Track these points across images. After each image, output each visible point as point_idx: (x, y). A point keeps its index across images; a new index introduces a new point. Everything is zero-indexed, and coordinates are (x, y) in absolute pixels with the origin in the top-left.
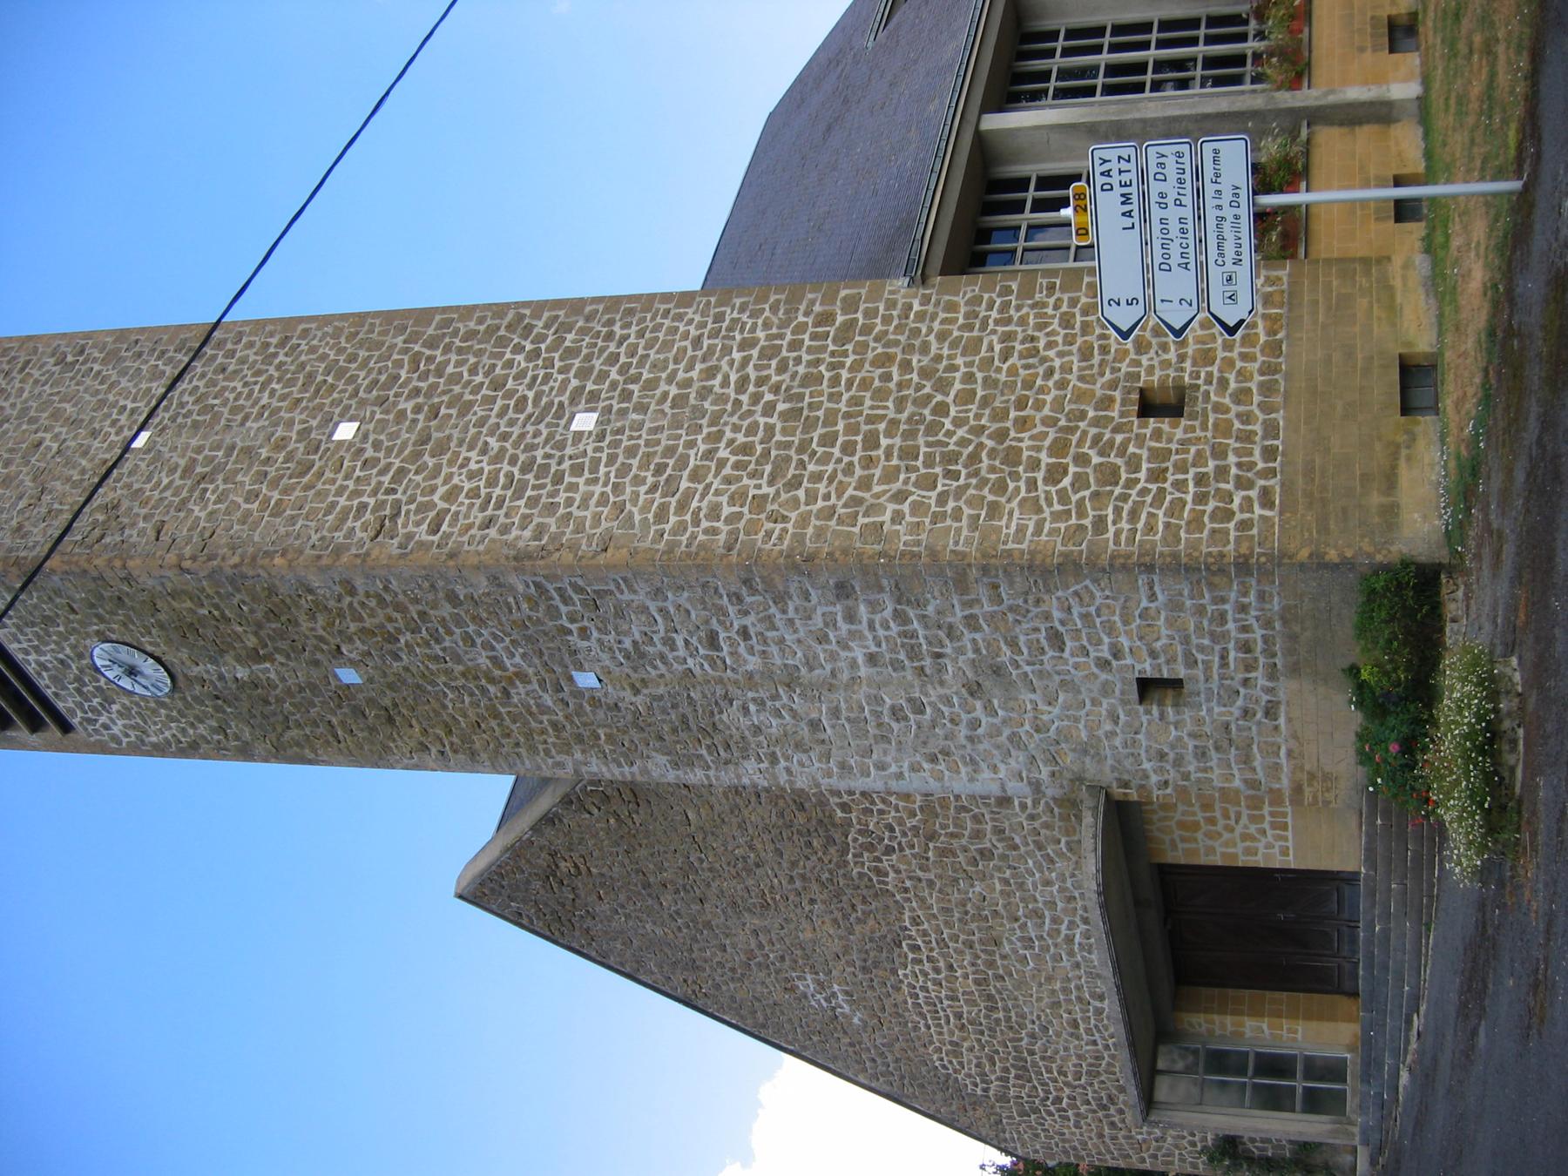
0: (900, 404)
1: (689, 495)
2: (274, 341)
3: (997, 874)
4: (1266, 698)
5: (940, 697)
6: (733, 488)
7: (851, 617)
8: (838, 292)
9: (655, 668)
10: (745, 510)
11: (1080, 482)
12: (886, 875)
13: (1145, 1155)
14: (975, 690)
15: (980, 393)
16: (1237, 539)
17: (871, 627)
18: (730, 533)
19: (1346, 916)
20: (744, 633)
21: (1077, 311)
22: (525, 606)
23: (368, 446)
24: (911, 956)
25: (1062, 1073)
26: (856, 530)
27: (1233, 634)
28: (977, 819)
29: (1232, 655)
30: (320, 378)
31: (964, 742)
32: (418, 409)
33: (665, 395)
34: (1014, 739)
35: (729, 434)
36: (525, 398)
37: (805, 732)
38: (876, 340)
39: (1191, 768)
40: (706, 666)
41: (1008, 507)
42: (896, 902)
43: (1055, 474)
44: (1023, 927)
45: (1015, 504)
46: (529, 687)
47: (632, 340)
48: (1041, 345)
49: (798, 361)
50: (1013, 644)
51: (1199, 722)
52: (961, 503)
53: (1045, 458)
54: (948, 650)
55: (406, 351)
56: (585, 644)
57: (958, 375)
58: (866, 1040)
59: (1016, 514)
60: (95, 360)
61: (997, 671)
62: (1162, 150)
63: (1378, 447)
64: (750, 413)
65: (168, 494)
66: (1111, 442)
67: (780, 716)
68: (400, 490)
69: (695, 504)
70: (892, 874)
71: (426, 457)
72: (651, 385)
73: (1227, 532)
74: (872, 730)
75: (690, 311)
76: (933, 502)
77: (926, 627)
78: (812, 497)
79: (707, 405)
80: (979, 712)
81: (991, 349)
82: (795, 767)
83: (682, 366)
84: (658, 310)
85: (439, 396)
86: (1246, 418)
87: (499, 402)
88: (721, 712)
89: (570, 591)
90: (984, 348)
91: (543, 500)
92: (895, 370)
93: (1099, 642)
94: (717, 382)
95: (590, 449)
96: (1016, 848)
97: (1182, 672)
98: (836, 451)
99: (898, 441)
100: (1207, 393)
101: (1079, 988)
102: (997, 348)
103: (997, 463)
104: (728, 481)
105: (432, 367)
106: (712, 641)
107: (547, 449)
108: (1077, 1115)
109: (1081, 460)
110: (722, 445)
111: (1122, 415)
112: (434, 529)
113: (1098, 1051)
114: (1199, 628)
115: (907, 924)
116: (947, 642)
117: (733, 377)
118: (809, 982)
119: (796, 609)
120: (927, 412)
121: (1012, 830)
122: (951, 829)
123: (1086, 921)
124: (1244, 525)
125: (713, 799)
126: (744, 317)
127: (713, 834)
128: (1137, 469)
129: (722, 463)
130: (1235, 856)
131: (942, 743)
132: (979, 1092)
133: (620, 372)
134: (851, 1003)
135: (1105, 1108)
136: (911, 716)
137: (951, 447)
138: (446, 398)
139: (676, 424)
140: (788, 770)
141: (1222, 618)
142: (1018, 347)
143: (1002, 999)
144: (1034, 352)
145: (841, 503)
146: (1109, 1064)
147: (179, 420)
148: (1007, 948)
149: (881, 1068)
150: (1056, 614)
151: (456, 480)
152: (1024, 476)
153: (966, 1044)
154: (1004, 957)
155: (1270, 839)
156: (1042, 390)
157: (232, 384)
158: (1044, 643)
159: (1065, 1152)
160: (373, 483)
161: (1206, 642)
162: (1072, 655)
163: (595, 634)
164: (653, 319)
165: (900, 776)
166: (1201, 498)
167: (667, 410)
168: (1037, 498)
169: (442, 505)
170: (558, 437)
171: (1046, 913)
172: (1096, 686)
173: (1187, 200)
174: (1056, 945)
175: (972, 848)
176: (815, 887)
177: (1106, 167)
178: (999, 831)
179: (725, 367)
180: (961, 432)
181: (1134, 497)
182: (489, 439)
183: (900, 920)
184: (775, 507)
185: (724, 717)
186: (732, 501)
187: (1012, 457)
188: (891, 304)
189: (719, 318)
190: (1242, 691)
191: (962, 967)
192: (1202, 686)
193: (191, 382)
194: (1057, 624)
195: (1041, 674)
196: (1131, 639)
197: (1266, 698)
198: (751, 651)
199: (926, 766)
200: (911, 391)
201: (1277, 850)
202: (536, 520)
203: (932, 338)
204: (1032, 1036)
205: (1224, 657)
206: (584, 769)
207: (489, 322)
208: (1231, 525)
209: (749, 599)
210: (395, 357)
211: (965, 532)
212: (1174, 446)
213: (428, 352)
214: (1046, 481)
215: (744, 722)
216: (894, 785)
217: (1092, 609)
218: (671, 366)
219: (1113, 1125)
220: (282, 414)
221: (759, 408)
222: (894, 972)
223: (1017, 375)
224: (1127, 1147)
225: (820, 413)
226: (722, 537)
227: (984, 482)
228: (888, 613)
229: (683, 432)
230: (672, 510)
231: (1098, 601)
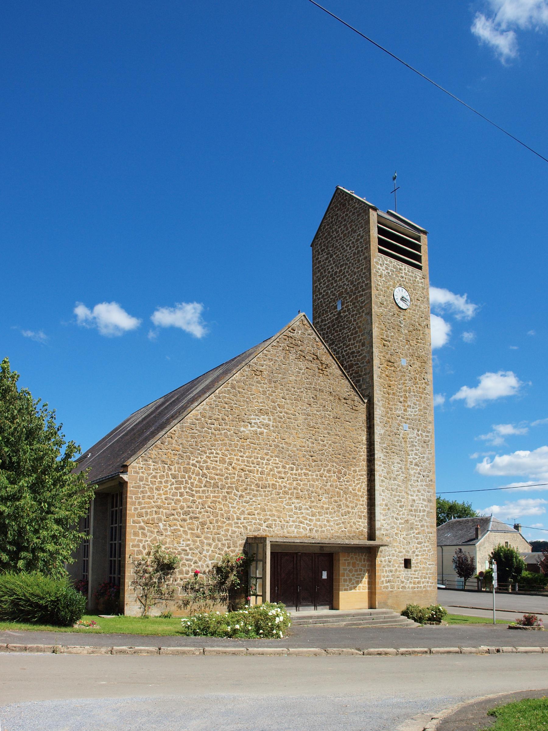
3: (331, 507)
5: (404, 513)
7: (423, 500)
9: (410, 447)
12: (327, 472)
14: (407, 521)
17: (422, 504)
24: (288, 466)
34: (393, 527)
46: (403, 410)
50: (419, 533)
54: (417, 519)
61: (412, 528)
80: (400, 521)
93: (419, 552)
106: (416, 465)
113: (233, 519)
114: (423, 573)
116: (419, 519)
122: (349, 499)
131: (391, 509)
136: (399, 504)
141: (425, 578)
150: (426, 544)
153: (230, 468)
154: (290, 498)
158: (419, 540)
162: (416, 546)
165: (381, 495)
171: (314, 518)
172: (408, 549)
176: (320, 447)
183: (307, 469)
185: (396, 457)
191: (282, 482)
192: (409, 573)
198: (415, 473)
201: (346, 588)
204: (241, 496)
209: (428, 479)
217: (427, 552)
222: (276, 456)
231: (429, 554)
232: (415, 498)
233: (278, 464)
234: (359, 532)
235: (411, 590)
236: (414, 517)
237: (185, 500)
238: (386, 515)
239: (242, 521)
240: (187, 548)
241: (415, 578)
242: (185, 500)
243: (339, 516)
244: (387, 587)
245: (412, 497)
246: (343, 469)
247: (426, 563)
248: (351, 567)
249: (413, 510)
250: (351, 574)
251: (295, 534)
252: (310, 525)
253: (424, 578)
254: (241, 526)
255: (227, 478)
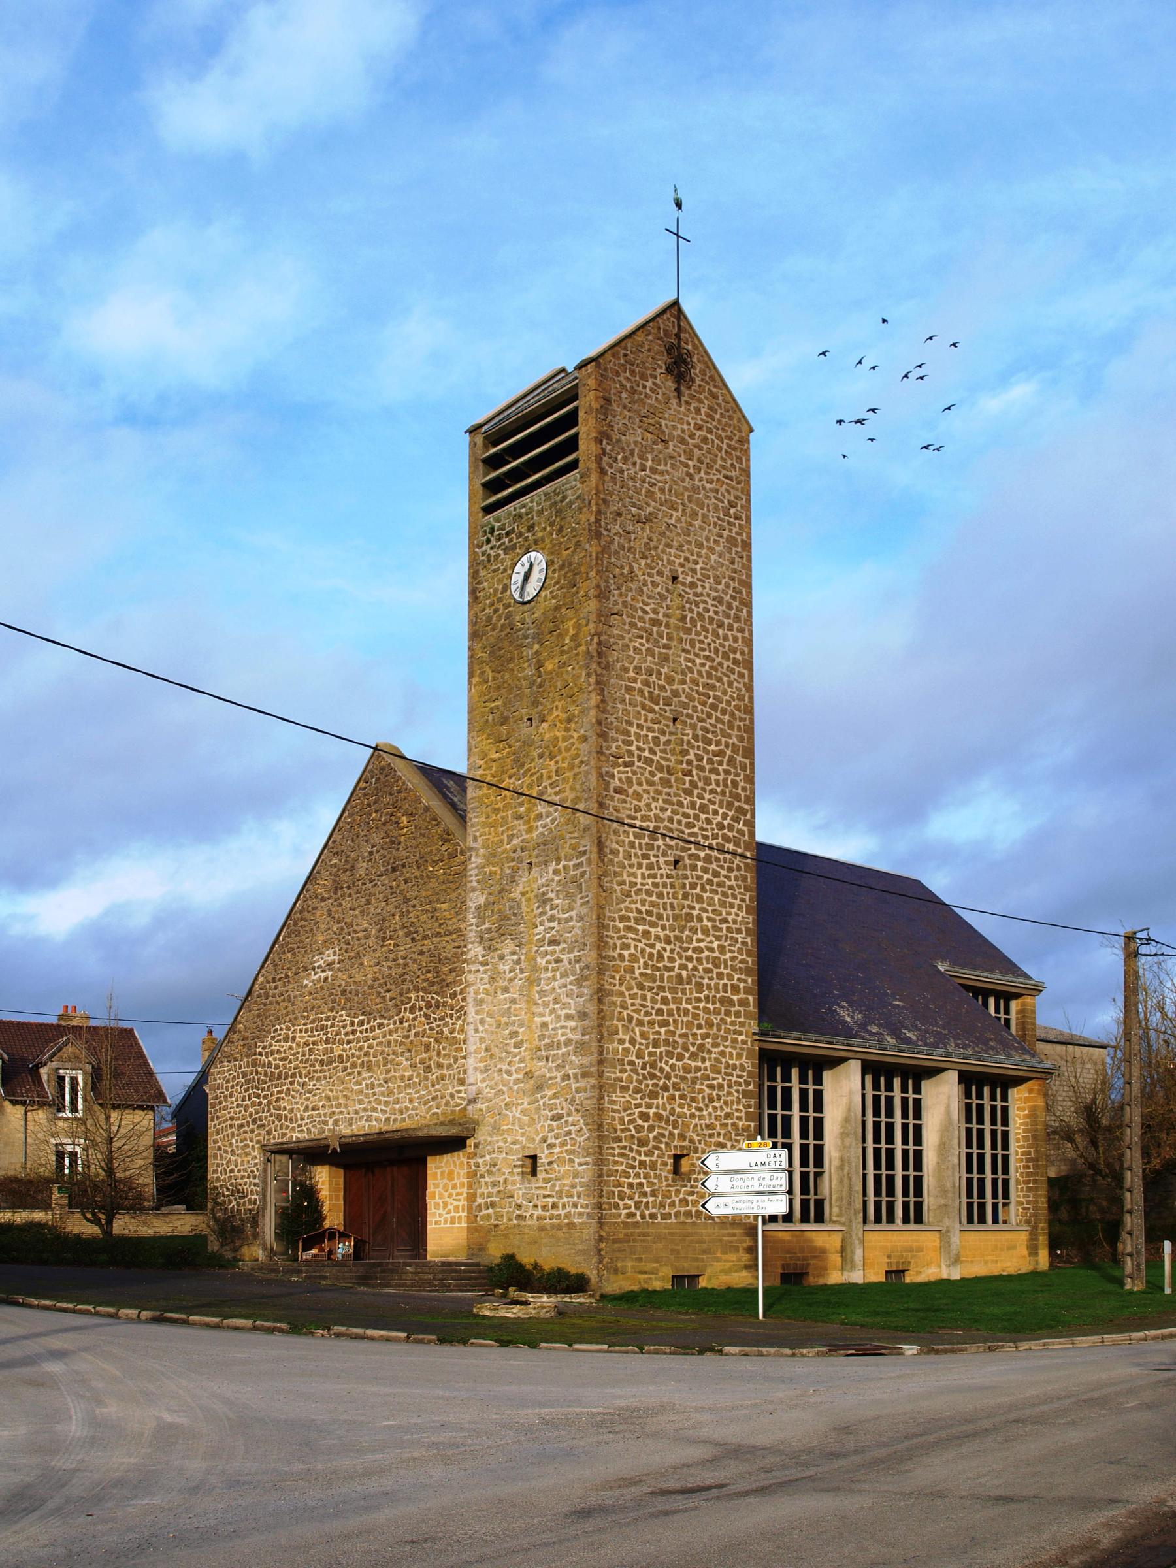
0: (684, 1036)
1: (636, 931)
2: (738, 656)
3: (415, 1074)
4: (528, 1215)
6: (639, 955)
7: (568, 1017)
8: (751, 994)
9: (538, 908)
10: (626, 963)
11: (639, 1129)
12: (411, 1012)
13: (220, 1144)
15: (688, 1076)
16: (610, 1203)
17: (563, 1027)
18: (614, 957)
19: (396, 1253)
20: (558, 961)
21: (735, 1120)
22: (573, 841)
23: (667, 737)
24: (356, 1020)
25: (278, 1100)
26: (615, 1022)
27: (562, 1201)
28: (450, 1066)
29: (550, 1200)
30: (711, 693)
31: (499, 1066)
32: (689, 763)
33: (693, 908)
34: (501, 1092)
35: (668, 948)
36: (694, 826)
37: (502, 983)
38: (722, 1019)
39: (487, 1179)
40: (538, 937)
41: (627, 1096)
42: (393, 1017)
43: (645, 1116)
44: (380, 1085)
45: (628, 1098)
47: (728, 883)
48: (715, 1104)
49: (711, 979)
50: (555, 1096)
51: (514, 1184)
52: (629, 1072)
53: (652, 1111)
55: (727, 746)
56: (551, 872)
57: (699, 1064)
58: (291, 986)
59: (623, 1099)
60: (730, 531)
62: (784, 1179)
63: (655, 1265)
64: (680, 958)
65: (640, 613)
66: (661, 1142)
67: (510, 972)
68: (640, 764)
69: (630, 935)
70: (411, 1016)
71: (659, 775)
72: (699, 899)
73: (614, 1198)
74: (504, 1020)
75: (744, 914)
76: (630, 1058)
77: (563, 1055)
78: (633, 997)
79: (687, 933)
80: (515, 1076)
81: (714, 1079)
82: (480, 975)
83: (711, 915)
84: (745, 895)
85: (697, 774)
86: (673, 1204)
87: (691, 812)
88: (512, 939)
89: (581, 870)
90: (714, 1076)
91: (633, 851)
92: (703, 1031)
93: (556, 1139)
94: (700, 936)
95: (662, 871)
96: (433, 1086)
97: (541, 1175)
98: (658, 1006)
99: (663, 1037)
100: (686, 1186)
101: (341, 1113)
102: (715, 1082)
103: (650, 1088)
104: (643, 951)
105: (716, 765)
106: (553, 942)
107: (663, 847)
108: (247, 1106)
109: (651, 1129)
110: (663, 945)
111: (675, 1147)
112: (617, 791)
114: (564, 1185)
115: (378, 1021)
117: (702, 945)
118: (332, 958)
119: (572, 990)
120: (679, 1050)
121: (444, 1085)
122: (443, 1052)
123: (387, 1119)
124: (617, 1206)
125: (455, 920)
126: (738, 945)
127: (432, 917)
128: (646, 1155)
129: (652, 946)
130: (433, 1197)
132: (258, 1050)
133: (708, 880)
134: (319, 980)
135: (254, 1121)
136: (513, 1041)
137: (659, 1064)
138: (696, 778)
139: (676, 918)
140: (478, 971)
142: (715, 1093)
143: (329, 1070)
144: (711, 1100)
145: (629, 1012)
146: (287, 1127)
147: (688, 606)
148: (365, 1075)
149: (271, 993)
150: (570, 1119)
151: (645, 796)
152: (643, 1102)
155: (445, 1216)
156: (690, 1106)
157: (709, 635)
159: (216, 1098)
160: (645, 746)
161: (557, 1188)
162: (549, 1125)
163: (557, 878)
164: (740, 893)
165: (476, 1031)
166: (631, 1185)
167: (684, 911)
168: (631, 1109)
169: (631, 791)
170: (669, 852)
173: (761, 1189)
174: (370, 1102)
175: (432, 1062)
176: (401, 971)
177: (778, 1156)
178: (443, 1078)
179: (708, 939)
180: (667, 1069)
181: (631, 1155)
182: (669, 810)
183: (383, 1017)
184: (627, 978)
186: (631, 955)
187: (654, 1095)
188: (742, 1024)
189: (739, 931)
190: (531, 1204)
191: (350, 1048)
193: (712, 605)
194: (565, 1119)
195: (538, 1108)
196: (558, 1153)
197: (528, 1215)
198: (548, 962)
199: (483, 1046)
200: (691, 1040)
201: (438, 1219)
202: (621, 849)
203: (722, 1048)
204: (304, 1084)
205: (549, 1196)
206: (474, 854)
207: (743, 794)
208: (617, 1200)
209: (577, 966)
210: (723, 740)
211: (613, 1076)
212: (658, 1172)
213: (725, 760)
214: (641, 1112)
215: (506, 952)
216: (470, 1029)
217: (573, 1136)
218: (710, 909)
219: (242, 1126)
220: (689, 675)
221: (684, 961)
223: (699, 1093)
224: (225, 1133)
225: (680, 995)
226: (611, 953)
227: (640, 1082)
228: (570, 1036)
229: (671, 922)
230: (627, 924)
231: (578, 1139)
232: (547, 1019)
233: (344, 1020)
234: (460, 1110)
235: (535, 1222)
236: (544, 1063)
237: (253, 1104)
238: (487, 1070)
239: (306, 1121)
240: (255, 1169)
241: (545, 1197)
242: (253, 1104)
243: (427, 1088)
244: (488, 1217)
245: (543, 1019)
246: (432, 998)
247: (574, 1162)
248: (445, 1181)
249: (542, 1047)
250: (446, 1194)
251: (367, 1131)
252: (386, 1112)
253: (567, 1197)
254: (305, 1129)
255: (290, 1062)
